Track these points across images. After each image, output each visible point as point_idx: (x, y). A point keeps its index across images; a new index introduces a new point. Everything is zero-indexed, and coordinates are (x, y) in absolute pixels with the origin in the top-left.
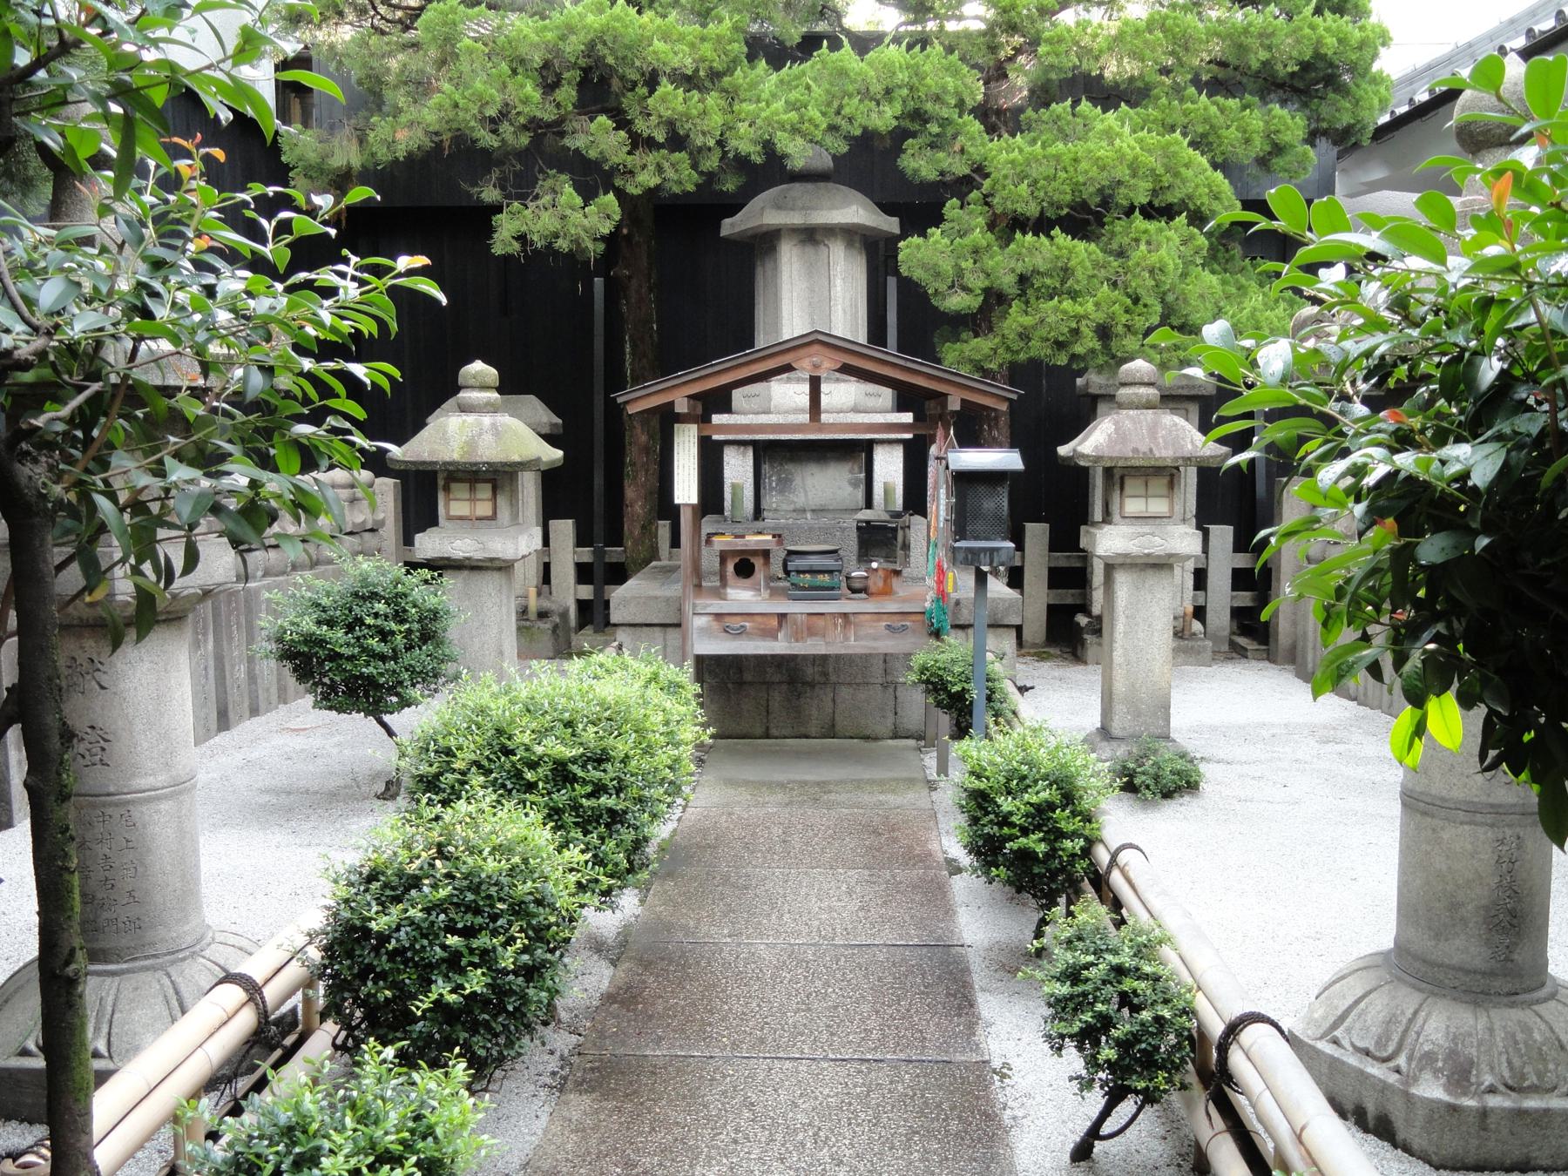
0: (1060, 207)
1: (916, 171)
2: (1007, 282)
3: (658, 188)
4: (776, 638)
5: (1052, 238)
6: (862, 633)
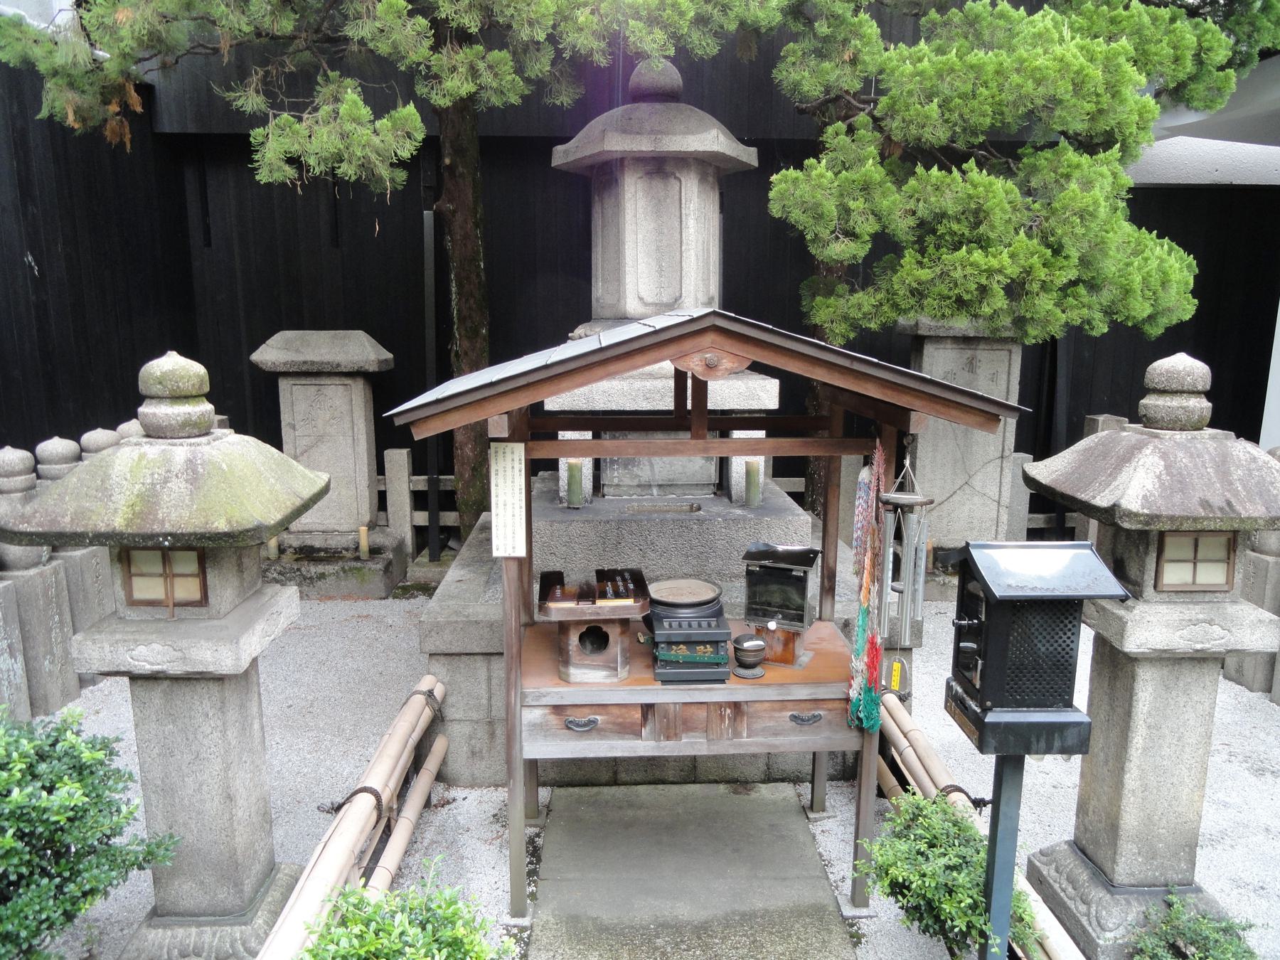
0: (974, 133)
1: (797, 85)
2: (902, 226)
3: (472, 98)
4: (638, 735)
5: (964, 173)
6: (758, 725)
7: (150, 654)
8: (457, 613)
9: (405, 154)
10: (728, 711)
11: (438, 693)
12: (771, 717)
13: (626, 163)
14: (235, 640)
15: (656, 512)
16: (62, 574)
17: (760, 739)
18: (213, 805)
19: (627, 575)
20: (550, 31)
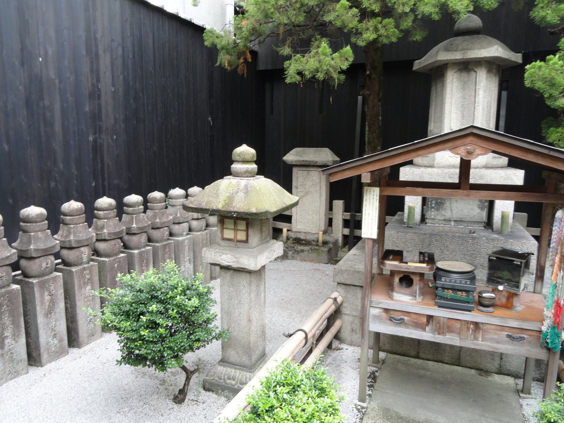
1: (544, 18)
3: (375, 41)
4: (424, 330)
6: (488, 336)
7: (226, 259)
8: (351, 267)
9: (344, 67)
10: (472, 326)
11: (339, 300)
12: (495, 334)
13: (449, 66)
14: (256, 257)
15: (451, 232)
16: (208, 236)
17: (489, 344)
18: (244, 322)
19: (426, 255)
20: (412, 7)
